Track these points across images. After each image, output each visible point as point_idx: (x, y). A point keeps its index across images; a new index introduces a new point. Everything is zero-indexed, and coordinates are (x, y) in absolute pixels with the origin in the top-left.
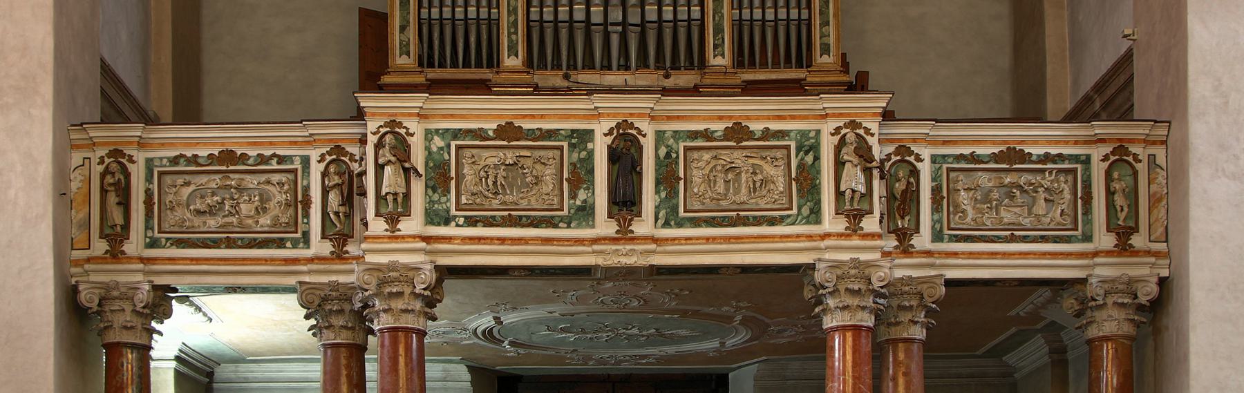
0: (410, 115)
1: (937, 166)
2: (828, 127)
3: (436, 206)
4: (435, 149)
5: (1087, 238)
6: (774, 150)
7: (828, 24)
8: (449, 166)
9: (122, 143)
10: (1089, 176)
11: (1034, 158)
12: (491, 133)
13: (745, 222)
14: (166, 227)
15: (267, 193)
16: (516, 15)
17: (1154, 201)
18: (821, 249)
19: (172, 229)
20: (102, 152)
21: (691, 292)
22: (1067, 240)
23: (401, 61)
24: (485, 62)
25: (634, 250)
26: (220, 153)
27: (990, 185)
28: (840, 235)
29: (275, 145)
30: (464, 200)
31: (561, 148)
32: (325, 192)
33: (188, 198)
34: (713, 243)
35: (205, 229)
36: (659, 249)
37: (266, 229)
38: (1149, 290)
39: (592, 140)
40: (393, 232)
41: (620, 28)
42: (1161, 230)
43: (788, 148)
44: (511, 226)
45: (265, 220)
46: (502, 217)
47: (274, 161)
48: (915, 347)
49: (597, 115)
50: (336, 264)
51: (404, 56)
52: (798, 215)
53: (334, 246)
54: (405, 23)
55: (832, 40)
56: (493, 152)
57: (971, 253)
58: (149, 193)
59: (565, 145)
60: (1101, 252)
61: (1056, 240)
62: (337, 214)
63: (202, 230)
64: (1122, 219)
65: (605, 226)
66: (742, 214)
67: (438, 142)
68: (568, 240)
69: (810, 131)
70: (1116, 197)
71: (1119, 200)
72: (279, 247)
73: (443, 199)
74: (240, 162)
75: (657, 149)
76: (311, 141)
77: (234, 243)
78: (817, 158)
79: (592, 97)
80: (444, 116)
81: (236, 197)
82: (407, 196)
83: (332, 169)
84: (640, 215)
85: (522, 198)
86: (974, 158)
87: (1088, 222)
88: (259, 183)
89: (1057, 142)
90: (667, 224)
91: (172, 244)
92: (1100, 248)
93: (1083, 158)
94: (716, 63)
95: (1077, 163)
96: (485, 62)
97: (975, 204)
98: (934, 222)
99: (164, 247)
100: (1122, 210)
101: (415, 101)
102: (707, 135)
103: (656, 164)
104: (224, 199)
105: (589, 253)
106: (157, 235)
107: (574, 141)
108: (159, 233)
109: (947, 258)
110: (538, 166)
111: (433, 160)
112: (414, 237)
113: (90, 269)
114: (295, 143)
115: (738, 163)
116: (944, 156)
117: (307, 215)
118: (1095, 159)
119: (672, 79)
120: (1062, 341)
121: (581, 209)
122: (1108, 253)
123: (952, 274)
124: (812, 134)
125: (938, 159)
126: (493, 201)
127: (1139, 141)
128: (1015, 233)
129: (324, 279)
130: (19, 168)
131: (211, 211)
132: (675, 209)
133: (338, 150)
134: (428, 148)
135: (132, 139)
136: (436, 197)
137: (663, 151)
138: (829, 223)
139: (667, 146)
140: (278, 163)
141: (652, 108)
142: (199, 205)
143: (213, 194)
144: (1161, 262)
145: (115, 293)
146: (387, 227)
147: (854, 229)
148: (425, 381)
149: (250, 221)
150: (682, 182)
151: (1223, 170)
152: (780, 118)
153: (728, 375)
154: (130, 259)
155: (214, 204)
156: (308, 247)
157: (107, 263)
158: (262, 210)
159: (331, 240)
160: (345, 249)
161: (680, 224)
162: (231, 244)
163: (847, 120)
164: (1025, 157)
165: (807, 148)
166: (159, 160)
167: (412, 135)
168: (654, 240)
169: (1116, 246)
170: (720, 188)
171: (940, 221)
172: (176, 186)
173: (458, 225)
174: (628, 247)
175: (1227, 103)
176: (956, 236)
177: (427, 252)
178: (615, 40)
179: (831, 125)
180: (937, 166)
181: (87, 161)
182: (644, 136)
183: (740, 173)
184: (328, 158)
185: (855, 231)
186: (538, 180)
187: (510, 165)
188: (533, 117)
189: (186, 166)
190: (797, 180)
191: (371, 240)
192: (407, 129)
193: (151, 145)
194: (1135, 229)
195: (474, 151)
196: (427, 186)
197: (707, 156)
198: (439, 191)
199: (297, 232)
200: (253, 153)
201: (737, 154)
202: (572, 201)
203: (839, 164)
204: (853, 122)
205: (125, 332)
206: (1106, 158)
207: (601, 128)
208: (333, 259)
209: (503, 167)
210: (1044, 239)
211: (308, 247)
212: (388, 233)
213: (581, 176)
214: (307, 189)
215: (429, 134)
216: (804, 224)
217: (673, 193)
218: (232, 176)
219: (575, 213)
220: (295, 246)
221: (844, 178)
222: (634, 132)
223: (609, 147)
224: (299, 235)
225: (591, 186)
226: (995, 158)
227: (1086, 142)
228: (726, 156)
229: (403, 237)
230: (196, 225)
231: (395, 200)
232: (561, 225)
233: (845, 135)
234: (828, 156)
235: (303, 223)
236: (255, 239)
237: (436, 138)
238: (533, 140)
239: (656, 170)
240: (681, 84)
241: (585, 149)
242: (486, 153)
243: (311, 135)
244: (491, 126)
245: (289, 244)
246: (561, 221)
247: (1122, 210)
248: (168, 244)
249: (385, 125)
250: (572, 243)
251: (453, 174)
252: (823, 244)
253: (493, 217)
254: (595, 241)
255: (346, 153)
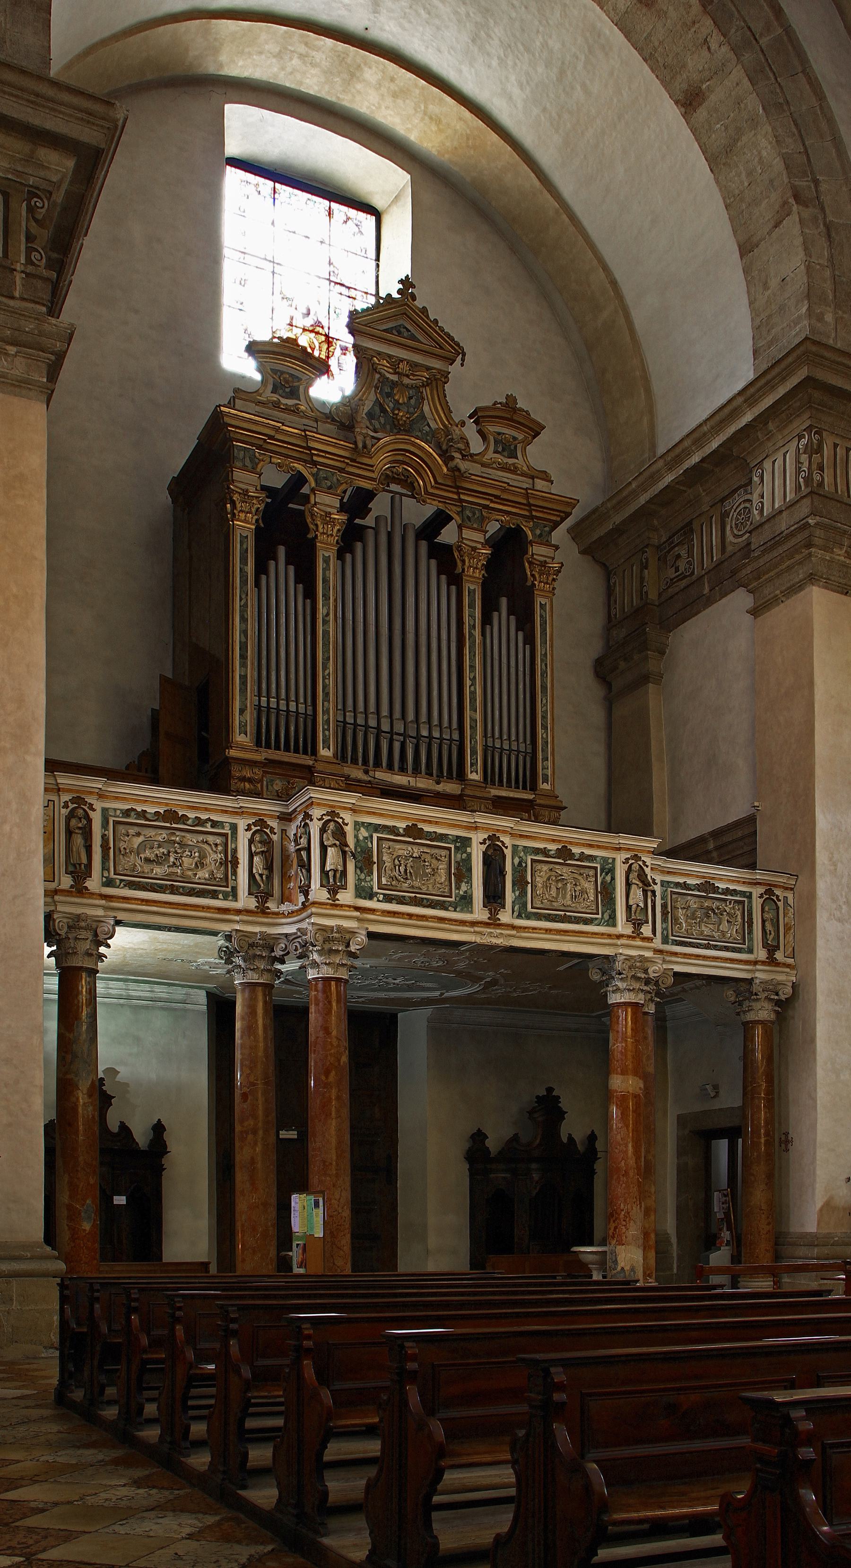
0: (345, 808)
1: (665, 889)
2: (620, 857)
3: (363, 883)
4: (361, 838)
5: (750, 951)
6: (587, 869)
7: (547, 760)
8: (372, 852)
9: (84, 792)
10: (751, 907)
11: (720, 890)
12: (401, 831)
13: (569, 920)
14: (120, 869)
15: (203, 851)
16: (329, 715)
17: (788, 928)
18: (618, 945)
19: (125, 872)
20: (66, 797)
21: (489, 961)
22: (739, 951)
23: (239, 738)
24: (301, 748)
25: (502, 934)
26: (165, 811)
27: (695, 906)
28: (629, 937)
29: (209, 811)
30: (384, 881)
31: (449, 849)
32: (251, 856)
33: (138, 847)
34: (550, 934)
35: (152, 875)
36: (518, 934)
37: (203, 881)
38: (786, 992)
39: (470, 846)
40: (334, 901)
41: (402, 738)
42: (791, 949)
43: (596, 868)
44: (416, 906)
45: (203, 874)
46: (410, 897)
47: (209, 825)
48: (650, 1018)
49: (475, 828)
50: (260, 917)
51: (242, 735)
52: (602, 919)
53: (258, 902)
54: (243, 707)
55: (549, 772)
56: (404, 846)
57: (685, 954)
58: (104, 838)
59: (452, 846)
60: (760, 961)
61: (734, 950)
62: (261, 875)
63: (150, 876)
64: (770, 939)
65: (480, 913)
66: (568, 914)
67: (364, 833)
68: (456, 921)
69: (609, 858)
70: (766, 923)
71: (768, 926)
72: (213, 898)
73: (368, 879)
74: (181, 822)
75: (513, 859)
76: (240, 812)
77: (177, 890)
78: (613, 879)
79: (474, 814)
80: (369, 813)
81: (179, 851)
82: (344, 873)
83: (257, 838)
84: (504, 907)
85: (424, 884)
86: (685, 886)
87: (751, 939)
88: (198, 842)
89: (733, 881)
90: (519, 916)
91: (125, 886)
92: (759, 959)
93: (748, 894)
94: (472, 778)
95: (744, 897)
96: (301, 748)
97: (687, 919)
98: (663, 929)
99: (118, 887)
100: (770, 934)
101: (350, 798)
102: (545, 852)
103: (513, 870)
104: (169, 852)
105: (471, 932)
106: (112, 875)
107: (458, 845)
108: (115, 874)
109: (671, 956)
110: (434, 861)
111: (360, 847)
112: (349, 906)
113: (59, 900)
114: (226, 812)
115: (565, 876)
116: (668, 882)
117: (235, 873)
118: (754, 896)
119: (441, 785)
120: (665, 1012)
121: (463, 898)
122: (763, 963)
123: (678, 968)
124: (610, 861)
125: (665, 884)
126: (403, 884)
127: (780, 887)
128: (711, 942)
129: (257, 929)
130: (14, 806)
131: (159, 860)
132: (525, 905)
133: (261, 823)
134: (356, 837)
135: (92, 790)
136: (362, 876)
137: (517, 860)
138: (622, 928)
139: (520, 857)
140: (212, 827)
141: (512, 828)
142: (148, 854)
143: (159, 846)
144: (792, 972)
145: (83, 924)
146: (329, 896)
147: (637, 934)
148: (95, 997)
149: (190, 873)
150: (530, 885)
151: (834, 915)
152: (591, 846)
153: (397, 1014)
154: (92, 895)
155: (161, 855)
156: (236, 900)
157: (73, 896)
158: (200, 865)
159: (256, 897)
160: (266, 905)
161: (528, 917)
162: (173, 890)
163: (633, 853)
164: (716, 890)
165: (607, 870)
166: (113, 811)
167: (347, 825)
168: (513, 927)
169: (767, 958)
170: (554, 892)
171: (666, 929)
172: (128, 836)
173: (378, 901)
174: (499, 931)
175: (836, 869)
176: (676, 941)
177: (359, 920)
178: (397, 746)
179: (625, 855)
180: (665, 889)
181: (51, 804)
182: (506, 848)
183: (566, 884)
184: (254, 829)
185: (638, 935)
186: (435, 871)
187: (416, 857)
188: (430, 822)
189: (136, 819)
190: (601, 893)
191: (317, 905)
192: (343, 819)
193: (106, 797)
194: (777, 947)
195: (391, 843)
196: (356, 867)
197: (545, 868)
198: (365, 871)
199: (228, 887)
200: (191, 815)
201: (565, 869)
202: (457, 891)
203: (628, 884)
204: (636, 855)
205: (86, 958)
206: (761, 896)
207: (477, 838)
208: (257, 913)
209: (411, 859)
210: (727, 949)
211: (236, 900)
212: (330, 901)
213: (463, 872)
214: (235, 851)
215: (357, 825)
216: (605, 926)
217: (523, 893)
218: (178, 833)
219: (460, 901)
220: (225, 899)
221: (631, 896)
222: (500, 844)
223: (484, 854)
224: (229, 889)
225: (470, 882)
226: (698, 887)
227: (749, 883)
228: (559, 869)
229: (342, 906)
230: (146, 871)
231: (335, 876)
232: (450, 908)
233: (632, 864)
234: (621, 878)
235: (232, 879)
236: (194, 889)
237: (362, 829)
238: (430, 840)
239: (513, 875)
240: (448, 790)
241: (465, 852)
242: (398, 846)
243: (241, 807)
244: (402, 825)
245: (221, 896)
246: (450, 906)
247: (770, 934)
248: (122, 885)
249: (328, 814)
250: (458, 923)
251: (375, 859)
252: (619, 942)
253: (404, 897)
254: (473, 924)
255: (267, 826)
